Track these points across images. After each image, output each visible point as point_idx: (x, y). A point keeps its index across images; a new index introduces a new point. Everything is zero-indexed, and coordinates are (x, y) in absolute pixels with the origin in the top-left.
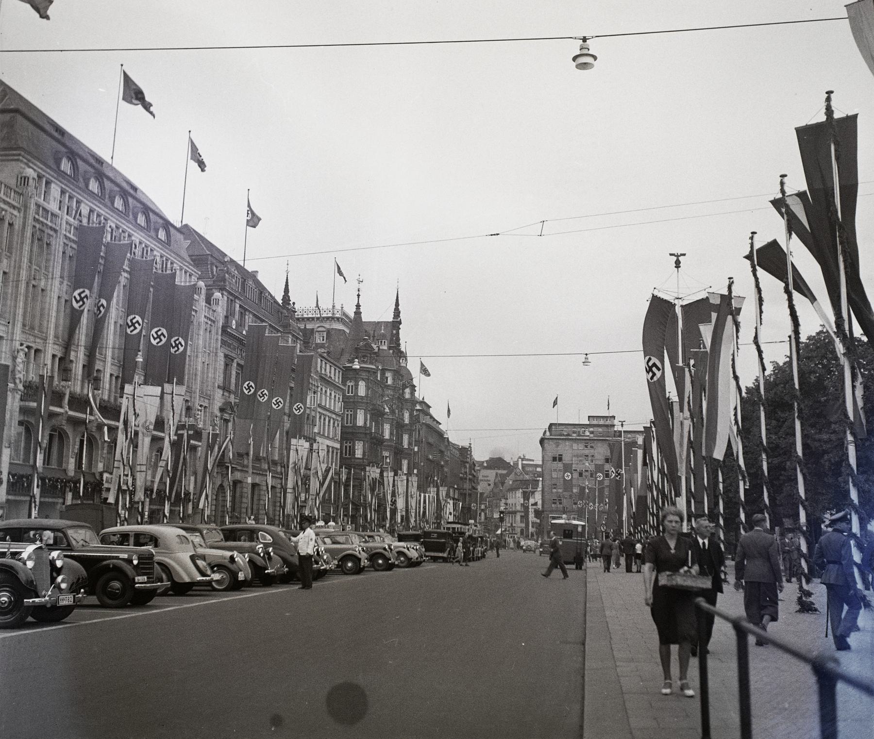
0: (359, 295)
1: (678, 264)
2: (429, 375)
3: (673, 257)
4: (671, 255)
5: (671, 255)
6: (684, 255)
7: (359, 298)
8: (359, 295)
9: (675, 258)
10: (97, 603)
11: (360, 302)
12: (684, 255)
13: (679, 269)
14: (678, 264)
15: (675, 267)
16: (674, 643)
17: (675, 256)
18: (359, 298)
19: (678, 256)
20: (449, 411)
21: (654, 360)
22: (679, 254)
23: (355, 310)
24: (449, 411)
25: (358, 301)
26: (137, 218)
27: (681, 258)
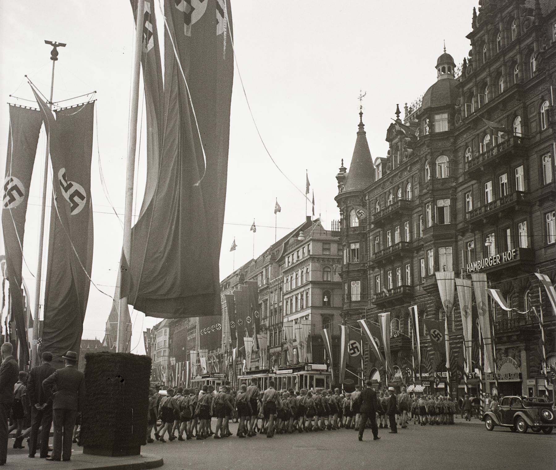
0: (361, 114)
1: (54, 56)
2: (474, 8)
3: (50, 45)
4: (47, 42)
5: (47, 42)
6: (64, 45)
7: (361, 116)
8: (361, 114)
9: (52, 48)
10: (413, 239)
11: (363, 121)
12: (64, 45)
13: (56, 62)
14: (54, 56)
15: (52, 59)
16: (47, 453)
17: (52, 45)
18: (361, 116)
19: (55, 45)
20: (308, 184)
21: (16, 182)
22: (57, 43)
23: (358, 130)
24: (308, 184)
25: (361, 118)
26: (150, 205)
27: (59, 49)
